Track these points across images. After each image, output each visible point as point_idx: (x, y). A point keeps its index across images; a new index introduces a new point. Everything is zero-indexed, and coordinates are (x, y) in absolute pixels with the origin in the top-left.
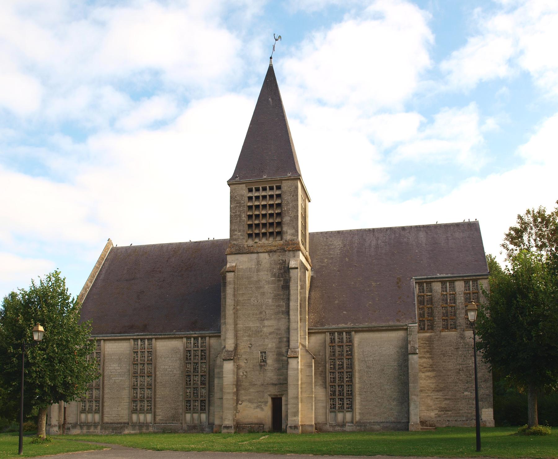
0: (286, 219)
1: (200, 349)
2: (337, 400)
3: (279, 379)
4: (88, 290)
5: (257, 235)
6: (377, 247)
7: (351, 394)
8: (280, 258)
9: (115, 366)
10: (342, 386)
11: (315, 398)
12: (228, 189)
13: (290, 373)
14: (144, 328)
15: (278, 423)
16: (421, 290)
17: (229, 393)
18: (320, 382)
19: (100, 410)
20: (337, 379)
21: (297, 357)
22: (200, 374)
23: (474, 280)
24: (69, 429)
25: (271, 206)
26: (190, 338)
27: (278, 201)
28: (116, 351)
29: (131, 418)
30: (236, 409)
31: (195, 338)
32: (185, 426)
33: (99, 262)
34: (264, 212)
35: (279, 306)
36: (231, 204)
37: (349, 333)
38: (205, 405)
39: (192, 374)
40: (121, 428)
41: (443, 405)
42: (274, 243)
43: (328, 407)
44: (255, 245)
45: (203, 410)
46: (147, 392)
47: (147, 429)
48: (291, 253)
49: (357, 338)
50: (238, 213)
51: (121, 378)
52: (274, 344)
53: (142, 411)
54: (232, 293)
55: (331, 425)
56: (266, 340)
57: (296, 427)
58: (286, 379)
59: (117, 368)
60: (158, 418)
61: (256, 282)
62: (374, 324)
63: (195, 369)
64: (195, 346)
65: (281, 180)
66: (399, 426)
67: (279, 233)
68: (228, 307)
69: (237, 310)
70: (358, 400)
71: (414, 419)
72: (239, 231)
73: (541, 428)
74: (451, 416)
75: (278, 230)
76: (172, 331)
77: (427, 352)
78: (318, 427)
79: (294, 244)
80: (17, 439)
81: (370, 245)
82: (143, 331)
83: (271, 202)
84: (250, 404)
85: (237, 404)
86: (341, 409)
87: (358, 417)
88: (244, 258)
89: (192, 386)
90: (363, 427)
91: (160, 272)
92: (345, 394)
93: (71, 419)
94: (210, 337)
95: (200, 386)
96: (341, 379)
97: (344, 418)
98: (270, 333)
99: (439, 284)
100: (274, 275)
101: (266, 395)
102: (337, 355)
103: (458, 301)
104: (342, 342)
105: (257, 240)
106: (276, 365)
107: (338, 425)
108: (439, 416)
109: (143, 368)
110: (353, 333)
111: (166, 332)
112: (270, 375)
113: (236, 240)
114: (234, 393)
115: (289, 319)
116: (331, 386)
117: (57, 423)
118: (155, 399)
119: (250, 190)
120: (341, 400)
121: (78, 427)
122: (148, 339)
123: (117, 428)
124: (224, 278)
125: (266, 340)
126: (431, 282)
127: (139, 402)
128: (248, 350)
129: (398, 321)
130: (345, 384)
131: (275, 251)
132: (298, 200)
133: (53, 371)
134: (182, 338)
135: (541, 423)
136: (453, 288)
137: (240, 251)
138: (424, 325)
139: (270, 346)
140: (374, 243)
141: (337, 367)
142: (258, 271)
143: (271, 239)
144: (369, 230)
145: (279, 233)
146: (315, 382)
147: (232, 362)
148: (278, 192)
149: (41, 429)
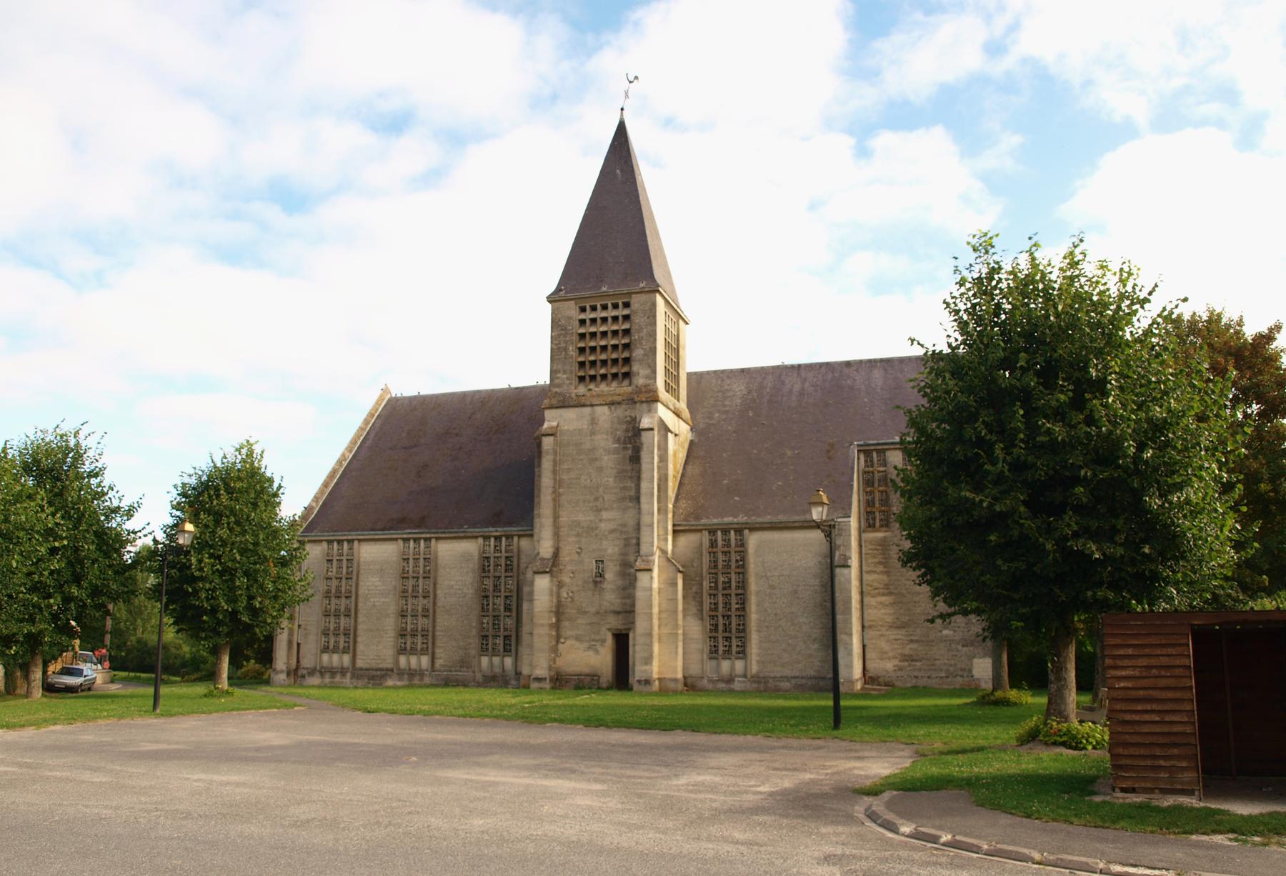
0: (638, 353)
1: (504, 554)
2: (720, 639)
4: (345, 464)
5: (593, 378)
6: (802, 393)
7: (743, 630)
8: (628, 413)
10: (729, 617)
11: (684, 634)
13: (640, 594)
14: (421, 523)
15: (622, 677)
16: (869, 462)
17: (542, 625)
18: (694, 610)
19: (351, 648)
20: (721, 606)
21: (650, 570)
22: (503, 594)
23: (878, 451)
24: (303, 677)
25: (615, 333)
26: (489, 537)
27: (626, 326)
29: (397, 662)
30: (554, 650)
31: (496, 538)
32: (479, 677)
33: (366, 422)
34: (603, 343)
37: (739, 531)
38: (511, 642)
39: (491, 594)
40: (382, 676)
41: (907, 651)
42: (621, 390)
43: (707, 650)
45: (507, 650)
46: (422, 622)
47: (421, 679)
48: (645, 405)
49: (753, 540)
50: (563, 345)
52: (617, 549)
53: (413, 651)
54: (551, 468)
55: (710, 681)
57: (648, 682)
58: (633, 605)
60: (439, 663)
61: (590, 450)
62: (781, 518)
63: (495, 586)
64: (496, 550)
65: (630, 294)
66: (822, 683)
67: (627, 375)
68: (543, 490)
69: (560, 495)
71: (853, 669)
72: (565, 372)
73: (1013, 694)
74: (920, 670)
75: (625, 370)
76: (461, 526)
77: (880, 563)
78: (689, 681)
79: (648, 392)
80: (151, 690)
81: (791, 391)
82: (419, 527)
83: (615, 328)
84: (577, 644)
85: (558, 642)
86: (728, 652)
87: (754, 668)
88: (570, 414)
89: (491, 613)
90: (762, 685)
91: (457, 435)
92: (734, 630)
93: (307, 662)
94: (519, 536)
95: (502, 613)
96: (727, 605)
97: (733, 668)
98: (611, 531)
100: (618, 441)
101: (604, 629)
102: (720, 567)
104: (729, 546)
105: (592, 386)
106: (619, 583)
107: (722, 680)
108: (901, 669)
109: (417, 584)
110: (746, 532)
111: (452, 527)
112: (610, 597)
113: (559, 386)
114: (551, 626)
116: (712, 617)
117: (284, 668)
118: (434, 632)
119: (583, 310)
120: (728, 639)
121: (318, 674)
122: (426, 539)
123: (375, 677)
124: (539, 445)
127: (408, 637)
128: (576, 557)
130: (733, 613)
131: (619, 403)
132: (655, 324)
133: (232, 589)
134: (476, 537)
135: (1014, 684)
138: (874, 519)
139: (610, 551)
140: (797, 387)
141: (720, 586)
142: (593, 433)
143: (614, 384)
144: (793, 366)
145: (627, 375)
146: (684, 610)
147: (548, 576)
148: (626, 312)
149: (220, 677)
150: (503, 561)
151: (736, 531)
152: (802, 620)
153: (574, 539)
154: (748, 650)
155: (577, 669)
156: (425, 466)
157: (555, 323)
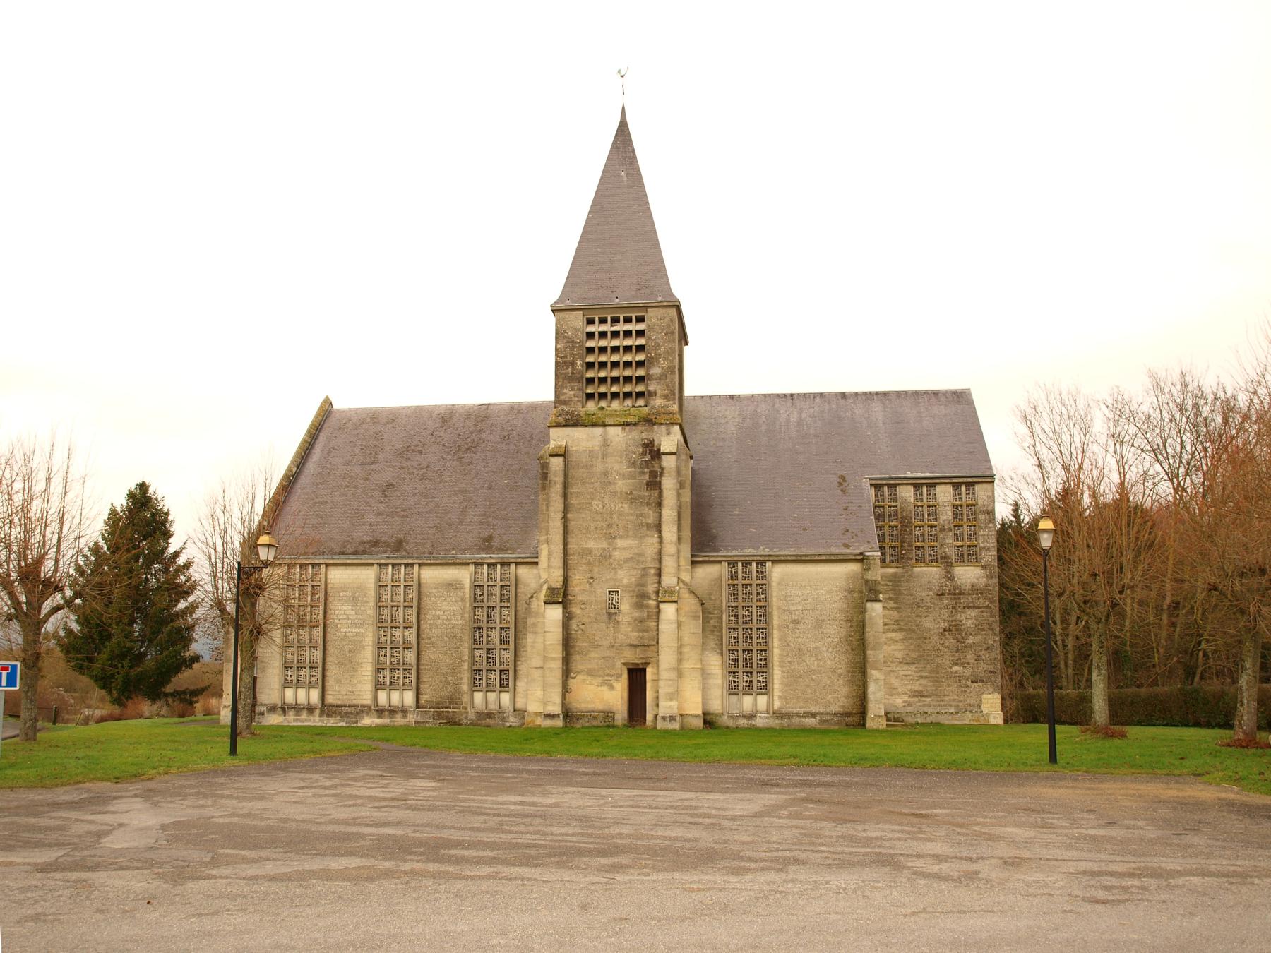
1: (499, 583)
3: (642, 638)
6: (800, 423)
7: (764, 667)
8: (644, 435)
12: (551, 320)
17: (554, 659)
23: (969, 485)
26: (509, 564)
28: (353, 583)
29: (375, 698)
31: (489, 565)
35: (641, 515)
36: (557, 343)
37: (761, 563)
40: (358, 713)
41: (917, 687)
44: (600, 413)
45: (504, 685)
48: (663, 428)
49: (777, 572)
53: (392, 686)
55: (731, 717)
56: (620, 572)
60: (424, 698)
62: (804, 551)
70: (777, 674)
71: (876, 709)
81: (788, 421)
82: (397, 550)
84: (589, 679)
86: (748, 690)
87: (777, 705)
91: (421, 452)
92: (755, 665)
95: (498, 646)
97: (755, 704)
98: (626, 561)
99: (949, 488)
100: (633, 464)
103: (942, 518)
104: (750, 578)
107: (744, 716)
108: (910, 705)
112: (627, 632)
115: (660, 537)
119: (591, 322)
122: (406, 565)
125: (620, 572)
126: (895, 485)
129: (846, 546)
131: (635, 424)
134: (468, 564)
136: (932, 496)
137: (573, 422)
152: (827, 655)
153: (584, 567)
155: (590, 706)
156: (391, 485)
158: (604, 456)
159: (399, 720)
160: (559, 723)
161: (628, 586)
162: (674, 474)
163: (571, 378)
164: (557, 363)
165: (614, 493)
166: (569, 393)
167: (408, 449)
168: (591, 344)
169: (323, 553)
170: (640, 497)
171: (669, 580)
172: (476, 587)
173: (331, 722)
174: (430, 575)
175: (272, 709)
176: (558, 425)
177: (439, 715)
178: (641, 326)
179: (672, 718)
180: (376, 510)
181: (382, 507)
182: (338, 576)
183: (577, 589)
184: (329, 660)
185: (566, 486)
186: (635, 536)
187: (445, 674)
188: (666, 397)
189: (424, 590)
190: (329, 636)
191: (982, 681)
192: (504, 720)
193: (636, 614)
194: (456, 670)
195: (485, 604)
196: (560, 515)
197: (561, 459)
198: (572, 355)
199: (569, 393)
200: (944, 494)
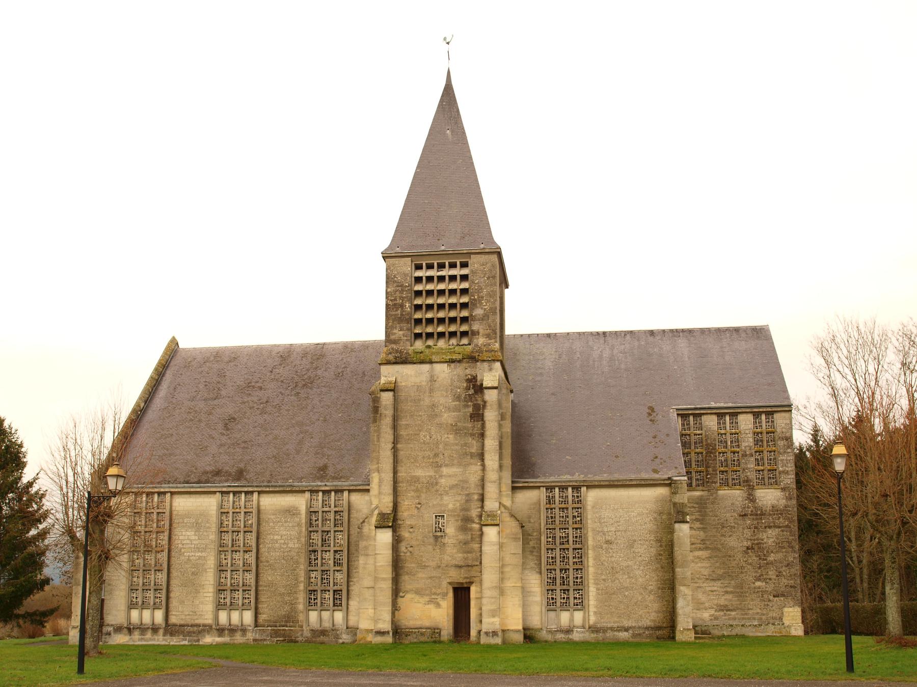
1: (333, 509)
6: (612, 359)
7: (580, 585)
9: (188, 533)
17: (384, 579)
18: (532, 564)
22: (332, 549)
29: (216, 618)
31: (324, 492)
37: (576, 488)
40: (200, 632)
41: (722, 602)
45: (337, 605)
48: (486, 365)
49: (591, 497)
51: (199, 554)
56: (446, 498)
59: (193, 537)
60: (262, 618)
62: (616, 476)
77: (697, 520)
81: (601, 357)
82: (238, 479)
84: (417, 598)
87: (593, 619)
91: (261, 388)
92: (571, 583)
97: (572, 619)
98: (452, 487)
100: (458, 398)
104: (566, 502)
107: (561, 631)
108: (716, 618)
112: (452, 554)
119: (419, 267)
122: (246, 493)
125: (446, 498)
131: (459, 361)
134: (304, 492)
140: (606, 354)
150: (331, 516)
151: (574, 488)
153: (412, 494)
154: (585, 602)
155: (418, 623)
157: (389, 280)
158: (431, 390)
159: (238, 638)
160: (389, 639)
161: (453, 510)
162: (495, 407)
163: (400, 320)
164: (387, 305)
165: (440, 425)
166: (398, 333)
167: (249, 385)
168: (419, 287)
169: (169, 482)
170: (465, 428)
171: (491, 505)
172: (311, 513)
173: (174, 641)
174: (269, 502)
175: (118, 629)
176: (388, 363)
177: (276, 633)
178: (465, 271)
179: (495, 633)
180: (219, 443)
181: (224, 439)
182: (182, 504)
183: (405, 514)
184: (172, 582)
185: (395, 419)
186: (460, 464)
187: (282, 595)
188: (488, 336)
189: (262, 516)
190: (173, 560)
191: (783, 595)
192: (337, 637)
193: (461, 537)
194: (292, 591)
195: (320, 528)
196: (390, 446)
197: (391, 394)
198: (401, 298)
199: (398, 333)
200: (746, 422)
